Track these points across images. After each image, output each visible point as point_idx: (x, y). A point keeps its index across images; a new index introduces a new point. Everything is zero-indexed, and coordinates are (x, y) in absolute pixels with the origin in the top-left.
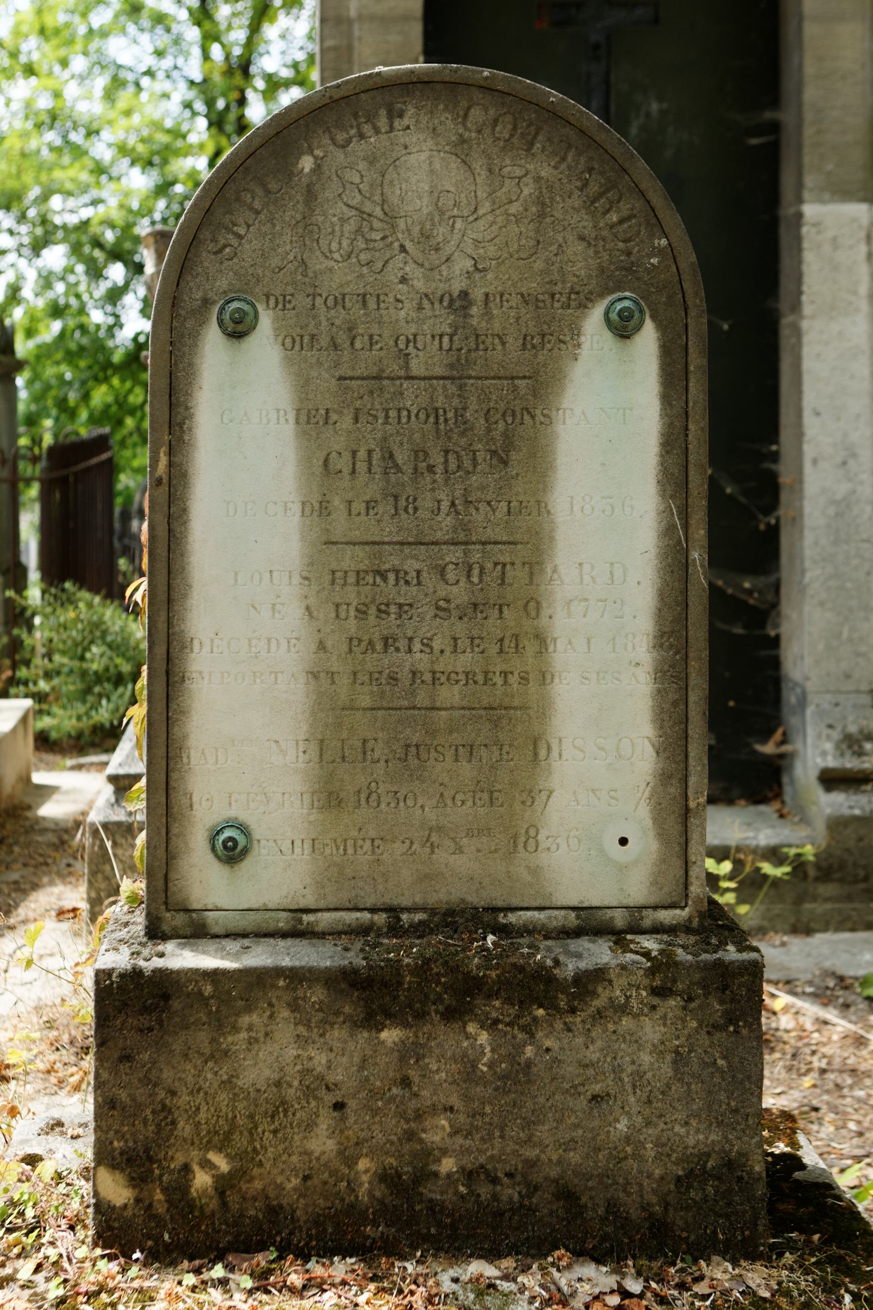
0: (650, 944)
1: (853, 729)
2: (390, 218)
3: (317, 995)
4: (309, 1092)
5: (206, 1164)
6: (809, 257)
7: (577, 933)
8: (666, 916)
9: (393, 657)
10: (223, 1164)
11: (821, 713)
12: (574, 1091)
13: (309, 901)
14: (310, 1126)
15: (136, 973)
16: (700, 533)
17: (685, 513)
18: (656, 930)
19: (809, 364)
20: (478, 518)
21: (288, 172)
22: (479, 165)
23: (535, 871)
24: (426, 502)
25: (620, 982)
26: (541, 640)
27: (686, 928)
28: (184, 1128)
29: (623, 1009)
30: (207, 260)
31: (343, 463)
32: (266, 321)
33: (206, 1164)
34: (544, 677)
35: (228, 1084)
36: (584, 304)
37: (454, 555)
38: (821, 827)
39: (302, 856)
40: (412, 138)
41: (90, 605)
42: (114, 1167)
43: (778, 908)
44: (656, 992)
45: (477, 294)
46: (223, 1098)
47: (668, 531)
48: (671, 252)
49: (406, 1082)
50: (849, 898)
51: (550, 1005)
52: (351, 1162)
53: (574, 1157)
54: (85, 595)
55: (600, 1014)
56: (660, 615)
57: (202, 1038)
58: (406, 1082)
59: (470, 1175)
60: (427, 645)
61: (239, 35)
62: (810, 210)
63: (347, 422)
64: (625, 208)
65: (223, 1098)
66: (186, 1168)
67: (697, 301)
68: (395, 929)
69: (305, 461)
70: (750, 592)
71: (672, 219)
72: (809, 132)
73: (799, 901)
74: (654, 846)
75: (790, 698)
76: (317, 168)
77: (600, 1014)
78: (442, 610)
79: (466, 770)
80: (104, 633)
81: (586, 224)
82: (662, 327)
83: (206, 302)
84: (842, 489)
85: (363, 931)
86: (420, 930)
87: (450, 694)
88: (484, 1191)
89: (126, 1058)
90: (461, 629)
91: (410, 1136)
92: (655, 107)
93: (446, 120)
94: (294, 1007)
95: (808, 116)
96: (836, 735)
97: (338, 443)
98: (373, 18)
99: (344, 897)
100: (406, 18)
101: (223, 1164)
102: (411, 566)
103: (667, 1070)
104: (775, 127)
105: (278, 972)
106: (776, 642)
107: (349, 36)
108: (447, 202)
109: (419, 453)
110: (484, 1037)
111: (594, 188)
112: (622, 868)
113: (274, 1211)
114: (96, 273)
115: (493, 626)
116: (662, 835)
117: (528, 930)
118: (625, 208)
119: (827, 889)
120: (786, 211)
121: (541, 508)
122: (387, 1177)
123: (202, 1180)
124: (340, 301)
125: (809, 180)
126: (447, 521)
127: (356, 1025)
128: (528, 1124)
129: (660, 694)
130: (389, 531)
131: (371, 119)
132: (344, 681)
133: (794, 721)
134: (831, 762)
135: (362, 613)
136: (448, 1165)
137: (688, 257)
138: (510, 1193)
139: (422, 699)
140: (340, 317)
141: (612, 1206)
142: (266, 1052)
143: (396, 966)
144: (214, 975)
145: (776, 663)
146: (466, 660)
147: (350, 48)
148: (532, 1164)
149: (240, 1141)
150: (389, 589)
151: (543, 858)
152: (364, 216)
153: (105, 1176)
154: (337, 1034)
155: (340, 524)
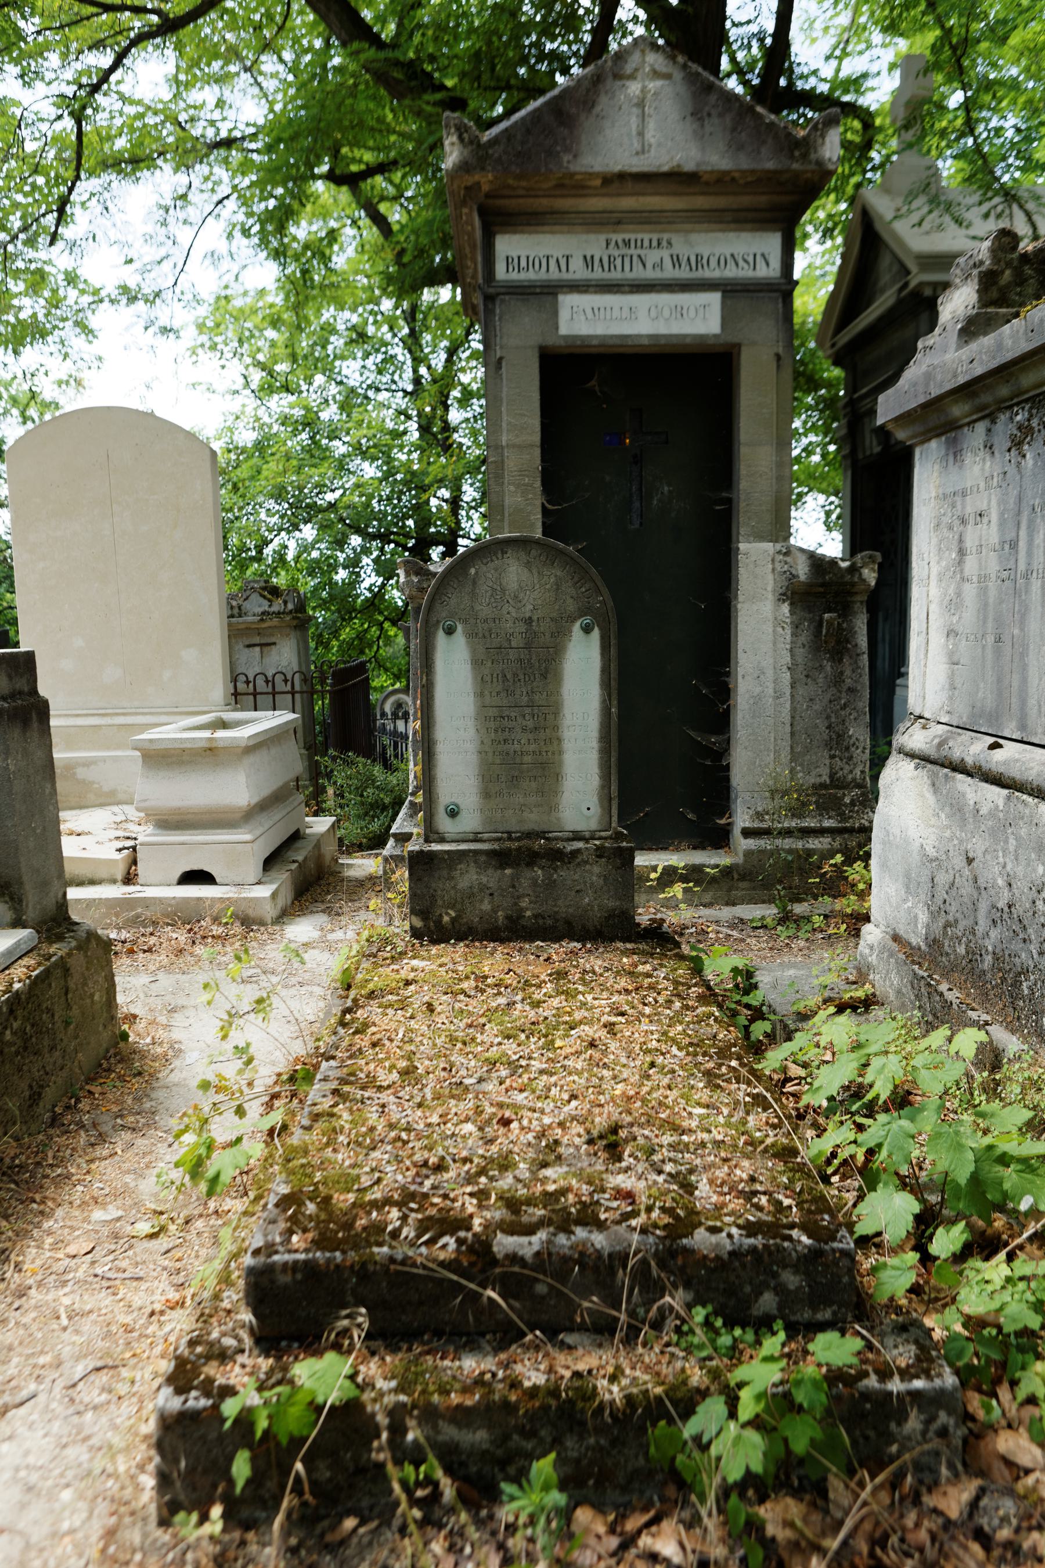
0: (597, 842)
1: (760, 809)
2: (503, 590)
3: (483, 858)
4: (481, 890)
5: (447, 914)
6: (741, 570)
7: (573, 839)
8: (603, 834)
9: (507, 746)
10: (453, 914)
11: (744, 802)
12: (570, 889)
13: (480, 830)
14: (482, 901)
15: (422, 851)
16: (615, 702)
17: (609, 696)
18: (599, 839)
19: (740, 627)
20: (536, 697)
21: (466, 573)
22: (535, 571)
23: (558, 819)
24: (518, 692)
25: (585, 854)
26: (559, 740)
27: (610, 837)
28: (440, 902)
29: (587, 862)
30: (438, 606)
31: (488, 679)
32: (460, 628)
33: (447, 914)
34: (561, 753)
35: (454, 888)
36: (573, 620)
37: (528, 710)
38: (741, 855)
39: (477, 814)
40: (510, 561)
41: (365, 765)
42: (416, 915)
43: (719, 894)
44: (597, 856)
45: (535, 618)
46: (452, 892)
47: (603, 702)
48: (604, 602)
49: (514, 887)
50: (754, 889)
51: (563, 861)
52: (496, 912)
53: (571, 910)
54: (361, 759)
55: (579, 864)
56: (601, 731)
57: (445, 873)
58: (514, 887)
59: (536, 916)
60: (519, 742)
61: (438, 361)
62: (742, 546)
63: (489, 664)
64: (587, 586)
65: (452, 892)
66: (441, 915)
67: (614, 620)
68: (510, 839)
69: (475, 678)
70: (714, 743)
71: (605, 591)
72: (742, 505)
73: (730, 890)
74: (599, 810)
75: (733, 796)
76: (477, 573)
77: (579, 864)
78: (524, 730)
79: (534, 785)
80: (374, 781)
81: (573, 592)
82: (601, 629)
83: (438, 622)
84: (758, 690)
85: (499, 839)
86: (518, 839)
87: (527, 759)
88: (541, 922)
89: (420, 880)
90: (531, 736)
91: (516, 904)
92: (666, 488)
93: (522, 554)
94: (475, 862)
95: (742, 497)
96: (751, 812)
97: (487, 672)
98: (514, 446)
99: (492, 828)
100: (532, 446)
101: (453, 914)
102: (513, 714)
103: (601, 882)
104: (729, 501)
105: (470, 851)
106: (727, 768)
107: (502, 455)
108: (523, 584)
109: (515, 675)
110: (540, 872)
111: (576, 579)
112: (588, 818)
113: (470, 929)
114: (340, 543)
115: (542, 735)
116: (602, 806)
117: (556, 839)
118: (587, 586)
119: (744, 884)
120: (733, 546)
121: (558, 693)
122: (508, 918)
123: (446, 919)
124: (486, 621)
125: (742, 531)
126: (525, 699)
127: (496, 868)
128: (555, 900)
129: (601, 758)
130: (505, 702)
131: (495, 554)
132: (490, 754)
133: (733, 806)
134: (747, 825)
135: (496, 731)
136: (528, 913)
137: (610, 603)
138: (549, 922)
139: (518, 761)
140: (486, 627)
141: (584, 927)
142: (466, 877)
143: (510, 849)
144: (448, 852)
145: (727, 779)
146: (533, 747)
147: (503, 461)
148: (556, 913)
149: (459, 906)
150: (505, 722)
151: (561, 815)
152: (494, 590)
153: (413, 918)
154: (490, 871)
155: (488, 700)
